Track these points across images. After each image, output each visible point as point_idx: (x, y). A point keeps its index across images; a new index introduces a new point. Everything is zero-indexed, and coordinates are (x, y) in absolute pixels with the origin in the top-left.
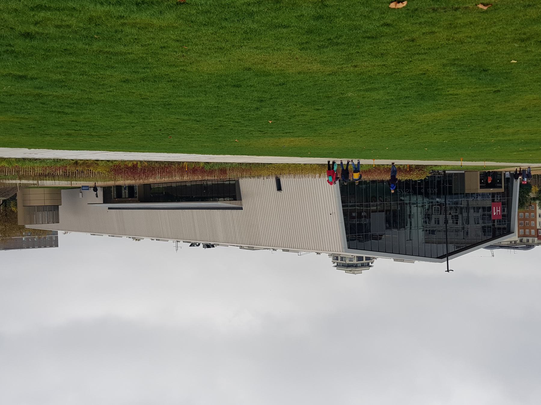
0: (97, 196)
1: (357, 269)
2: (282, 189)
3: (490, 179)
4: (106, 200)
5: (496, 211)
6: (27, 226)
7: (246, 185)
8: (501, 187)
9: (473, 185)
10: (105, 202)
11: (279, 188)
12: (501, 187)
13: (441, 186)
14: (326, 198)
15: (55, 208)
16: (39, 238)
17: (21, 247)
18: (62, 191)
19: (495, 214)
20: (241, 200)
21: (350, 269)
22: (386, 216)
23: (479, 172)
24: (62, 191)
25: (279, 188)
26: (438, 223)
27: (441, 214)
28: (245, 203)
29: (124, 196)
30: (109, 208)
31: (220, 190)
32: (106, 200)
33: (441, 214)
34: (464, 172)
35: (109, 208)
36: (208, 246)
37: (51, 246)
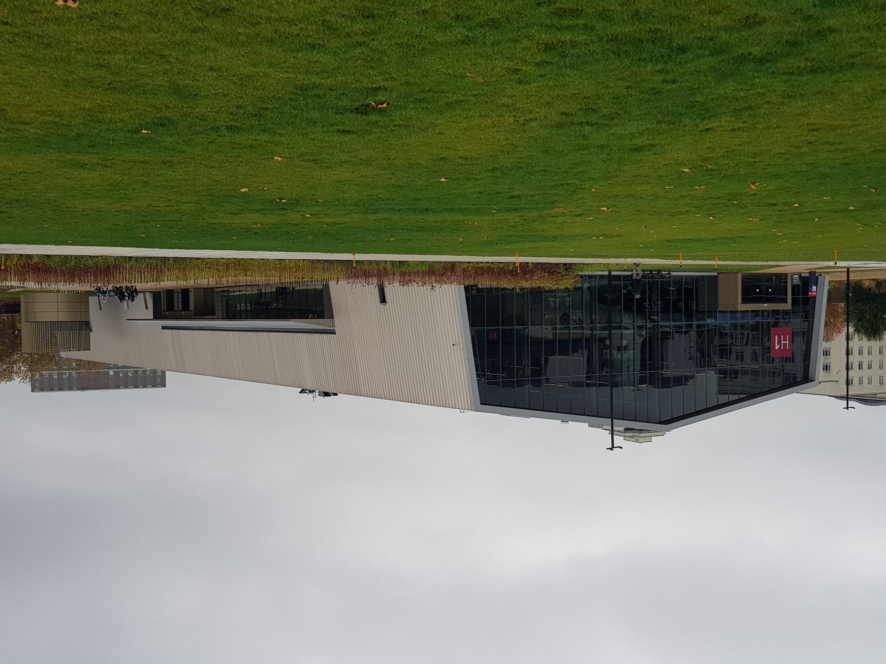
0: (147, 308)
1: (642, 435)
2: (387, 300)
3: (758, 287)
4: (158, 315)
5: (779, 343)
6: (63, 354)
7: (344, 294)
8: (785, 301)
9: (731, 297)
10: (157, 316)
11: (383, 300)
12: (785, 301)
13: (673, 299)
14: (440, 318)
15: (86, 326)
16: (41, 375)
17: (106, 387)
18: (90, 298)
19: (777, 347)
20: (332, 317)
21: (631, 434)
22: (588, 348)
23: (740, 275)
24: (90, 298)
25: (383, 300)
26: (742, 360)
27: (747, 344)
28: (339, 322)
29: (176, 309)
30: (164, 328)
31: (302, 305)
32: (158, 315)
33: (747, 344)
34: (716, 274)
35: (164, 328)
36: (326, 394)
37: (154, 386)
